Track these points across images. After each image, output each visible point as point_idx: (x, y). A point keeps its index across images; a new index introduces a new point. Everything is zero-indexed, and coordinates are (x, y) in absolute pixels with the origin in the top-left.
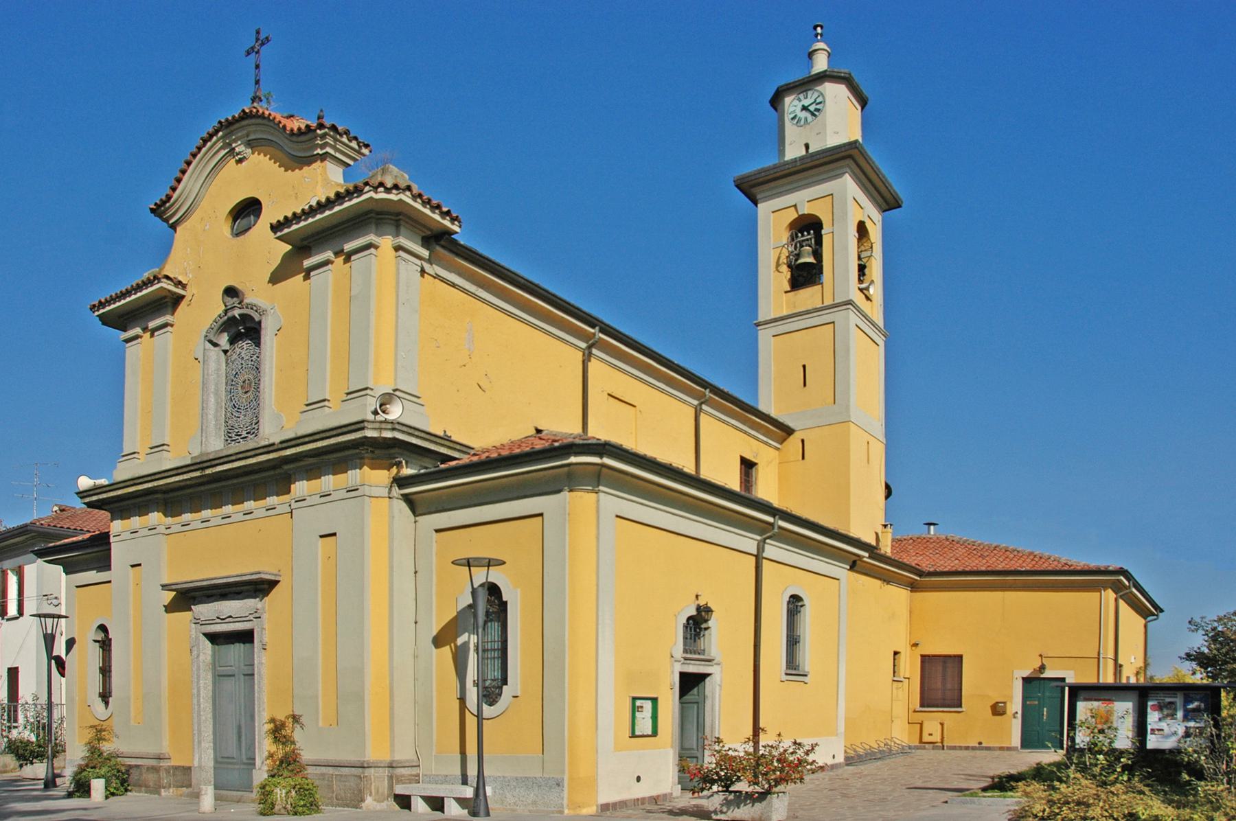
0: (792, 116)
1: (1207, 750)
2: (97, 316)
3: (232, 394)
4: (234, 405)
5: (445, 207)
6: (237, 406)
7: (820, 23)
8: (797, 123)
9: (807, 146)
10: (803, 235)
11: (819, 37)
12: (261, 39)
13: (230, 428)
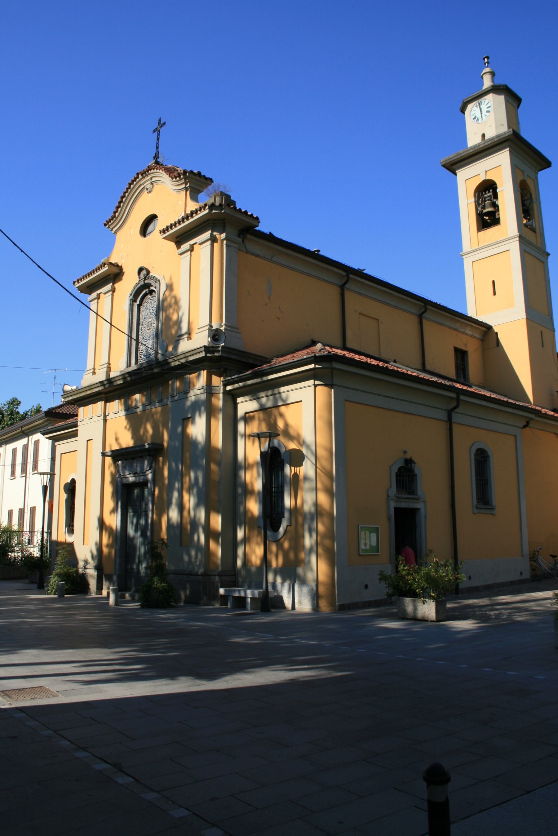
0: (473, 117)
1: (428, 571)
2: (77, 288)
3: (142, 331)
4: (143, 337)
5: (249, 212)
6: (145, 338)
7: (485, 56)
8: (477, 121)
9: (483, 136)
10: (486, 194)
11: (487, 65)
12: (161, 124)
13: (141, 351)
